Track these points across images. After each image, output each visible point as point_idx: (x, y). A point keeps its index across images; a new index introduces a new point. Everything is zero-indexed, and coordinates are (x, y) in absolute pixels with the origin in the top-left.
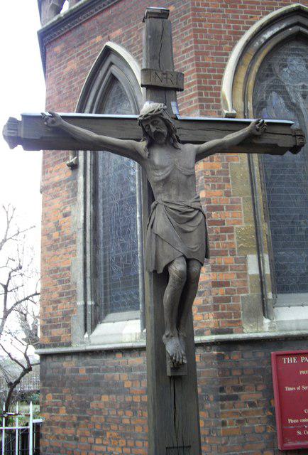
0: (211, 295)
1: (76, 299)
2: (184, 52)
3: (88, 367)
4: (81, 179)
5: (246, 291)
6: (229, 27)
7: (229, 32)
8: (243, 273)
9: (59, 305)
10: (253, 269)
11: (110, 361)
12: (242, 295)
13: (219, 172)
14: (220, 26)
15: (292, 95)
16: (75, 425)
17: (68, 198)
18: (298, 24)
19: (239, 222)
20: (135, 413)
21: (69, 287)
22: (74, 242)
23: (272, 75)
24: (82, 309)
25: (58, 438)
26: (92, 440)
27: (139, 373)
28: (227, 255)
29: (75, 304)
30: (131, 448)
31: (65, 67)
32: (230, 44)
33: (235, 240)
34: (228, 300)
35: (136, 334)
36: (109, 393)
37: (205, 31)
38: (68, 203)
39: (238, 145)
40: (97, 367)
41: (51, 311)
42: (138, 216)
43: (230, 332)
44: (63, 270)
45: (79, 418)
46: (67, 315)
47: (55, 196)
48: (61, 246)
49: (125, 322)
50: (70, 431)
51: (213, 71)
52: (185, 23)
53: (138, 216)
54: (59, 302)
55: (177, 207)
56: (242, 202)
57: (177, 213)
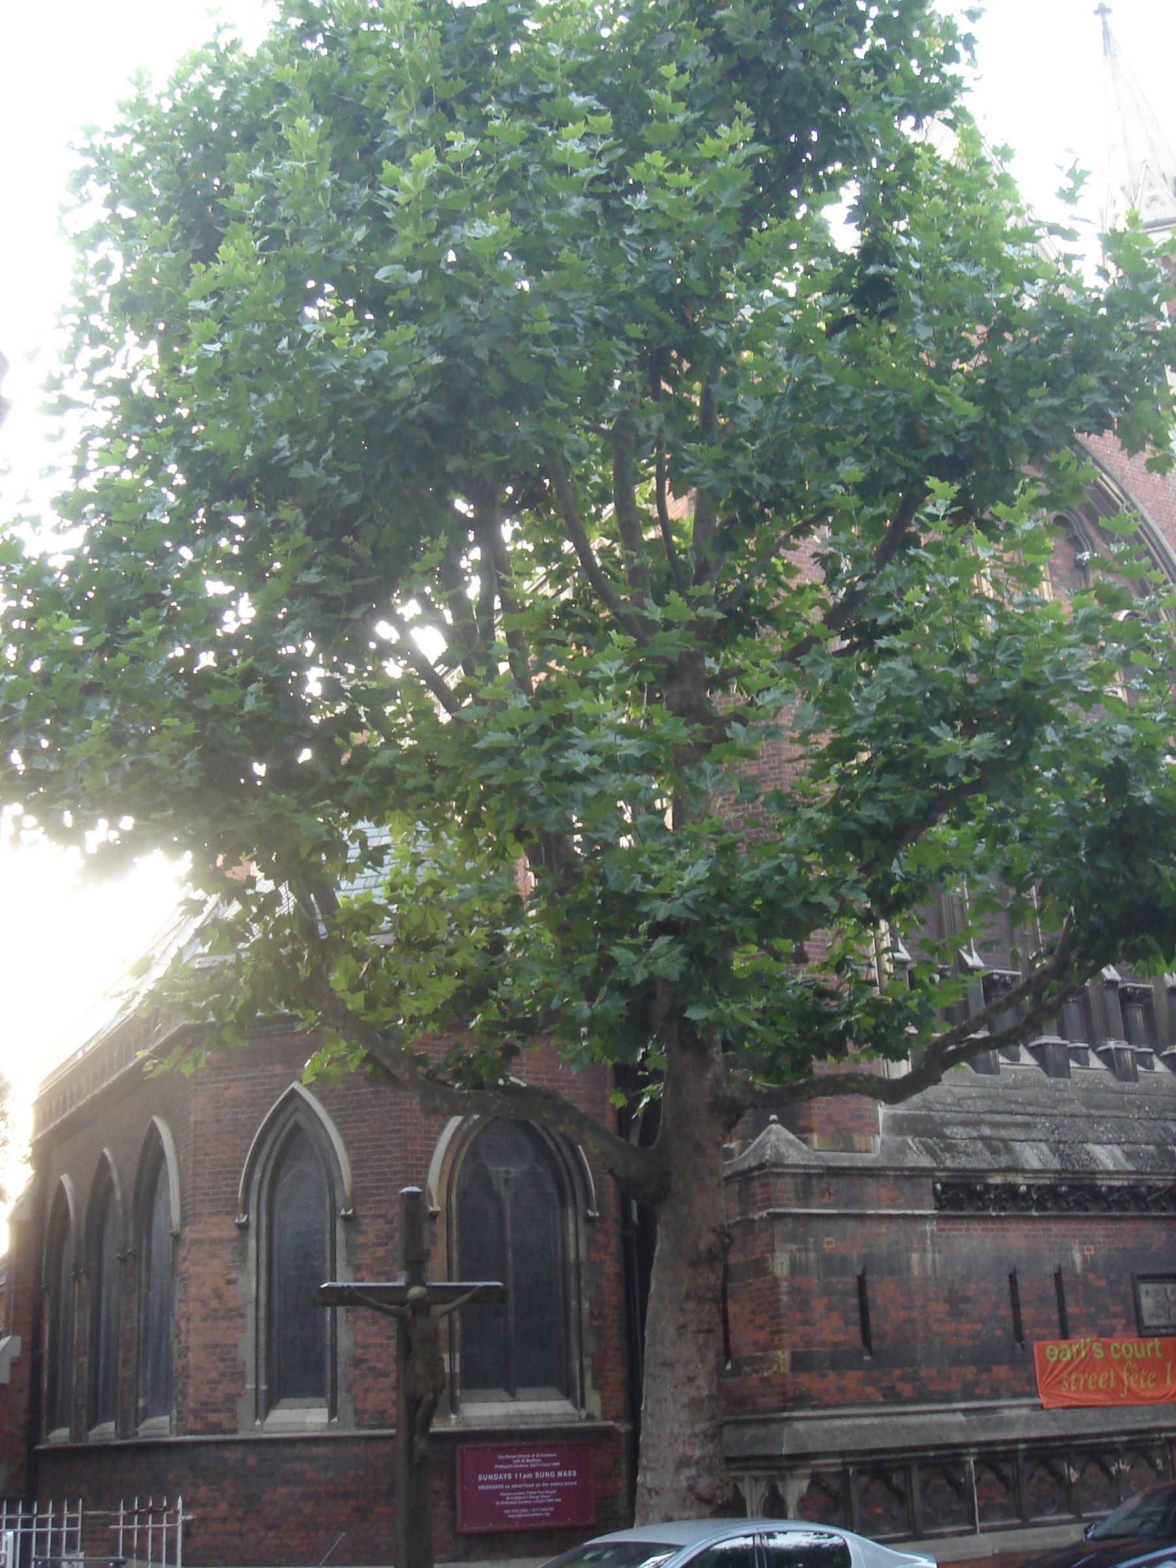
4: (252, 1243)
29: (243, 1387)
31: (227, 1088)
41: (207, 1392)
44: (226, 1346)
45: (246, 1513)
46: (231, 1399)
47: (213, 1256)
48: (223, 1318)
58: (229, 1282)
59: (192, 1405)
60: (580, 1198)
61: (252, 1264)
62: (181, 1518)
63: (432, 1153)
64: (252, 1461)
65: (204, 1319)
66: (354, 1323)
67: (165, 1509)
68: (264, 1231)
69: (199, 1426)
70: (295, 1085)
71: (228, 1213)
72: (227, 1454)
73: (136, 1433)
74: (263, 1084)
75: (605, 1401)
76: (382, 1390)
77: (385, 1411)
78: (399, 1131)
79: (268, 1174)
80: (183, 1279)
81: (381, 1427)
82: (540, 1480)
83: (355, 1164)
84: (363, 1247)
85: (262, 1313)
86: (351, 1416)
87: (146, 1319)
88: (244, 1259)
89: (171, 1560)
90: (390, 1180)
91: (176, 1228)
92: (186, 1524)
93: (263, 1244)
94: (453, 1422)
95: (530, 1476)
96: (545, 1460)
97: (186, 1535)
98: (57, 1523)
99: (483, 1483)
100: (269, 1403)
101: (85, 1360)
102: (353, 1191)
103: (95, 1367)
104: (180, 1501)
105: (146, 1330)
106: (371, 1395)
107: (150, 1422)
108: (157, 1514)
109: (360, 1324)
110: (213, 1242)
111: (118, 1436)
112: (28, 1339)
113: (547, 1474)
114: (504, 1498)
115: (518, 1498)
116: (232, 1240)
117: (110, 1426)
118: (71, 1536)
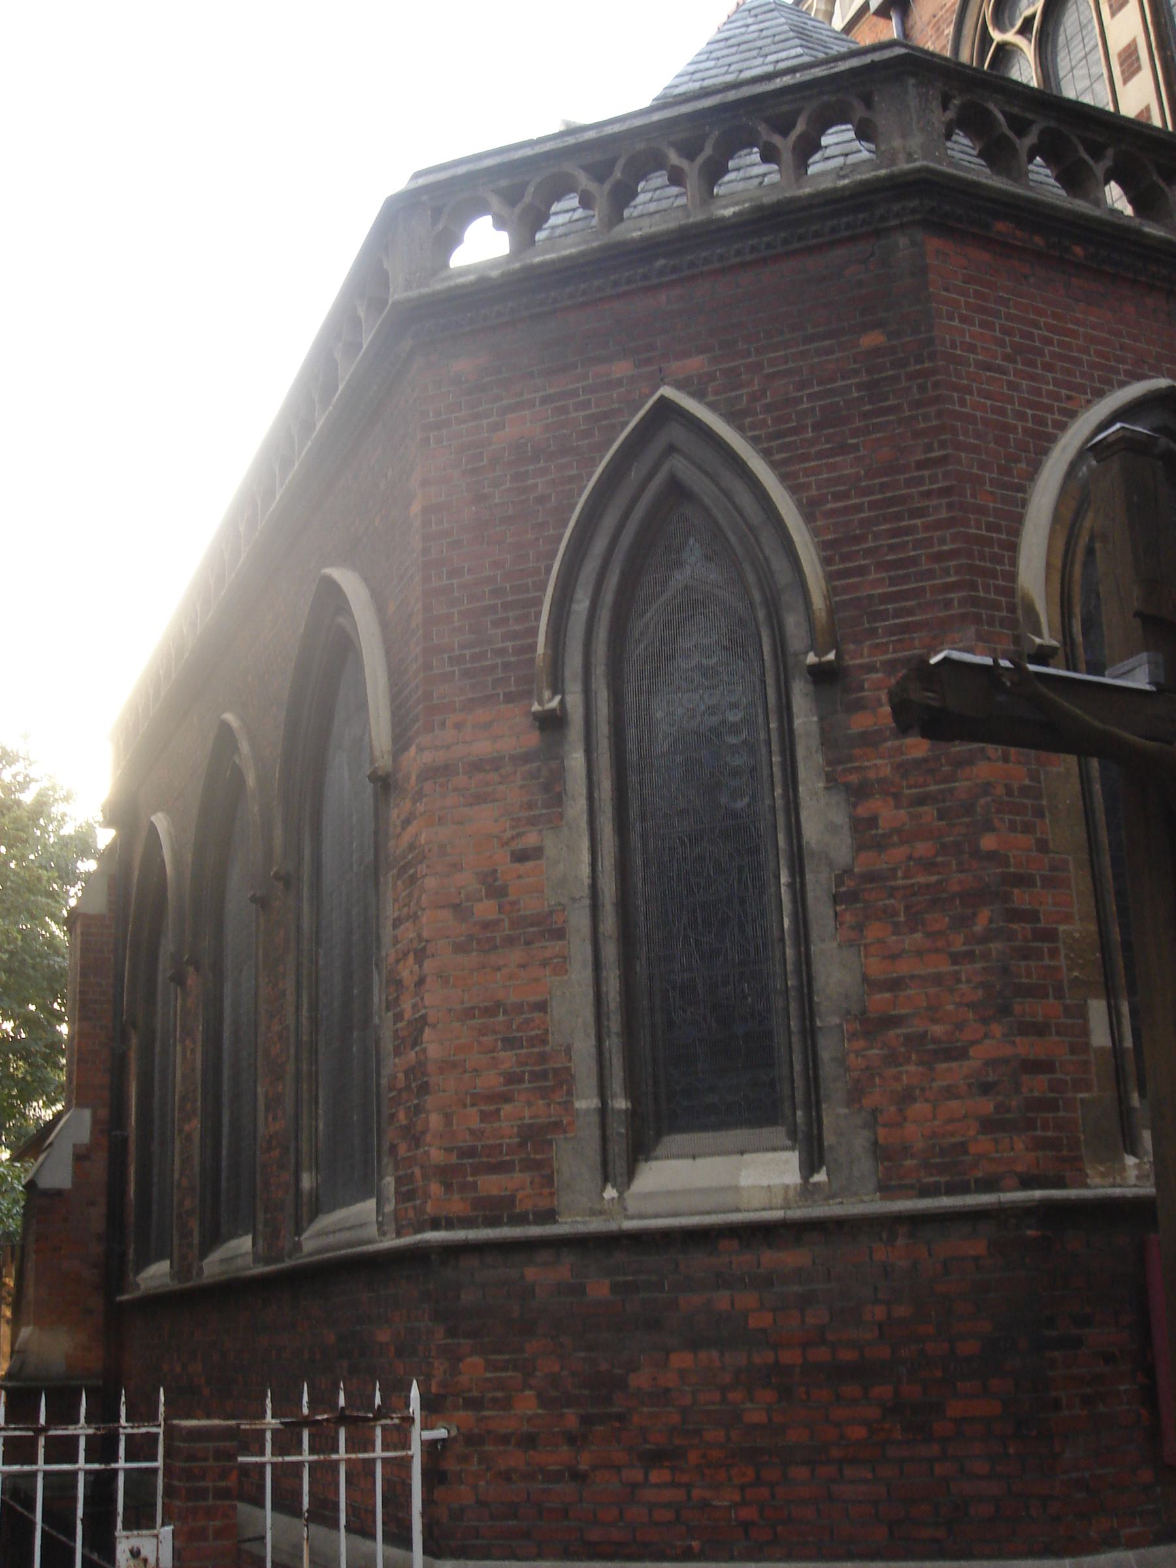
1: (570, 1093)
2: (920, 465)
3: (620, 1279)
4: (576, 759)
5: (1088, 1088)
6: (1022, 416)
7: (1025, 430)
8: (1081, 1044)
9: (507, 1109)
10: (1100, 1037)
11: (699, 1262)
12: (1081, 1095)
13: (1024, 791)
16: (571, 1439)
17: (530, 806)
19: (1067, 918)
21: (543, 1058)
22: (559, 934)
24: (595, 1119)
25: (509, 1479)
26: (636, 1475)
27: (797, 1289)
28: (1046, 996)
29: (567, 1105)
31: (497, 427)
32: (1028, 464)
33: (1062, 962)
34: (1052, 1105)
35: (787, 1187)
36: (694, 1345)
41: (475, 1123)
42: (784, 879)
43: (1061, 1184)
44: (519, 1008)
45: (587, 1420)
46: (537, 1139)
47: (481, 799)
48: (510, 941)
49: (735, 1158)
50: (558, 1457)
51: (998, 529)
52: (922, 388)
53: (784, 879)
54: (506, 1098)
56: (1071, 867)
58: (521, 856)
59: (437, 1155)
61: (577, 808)
62: (418, 1436)
63: (1019, 519)
64: (599, 1289)
66: (859, 928)
67: (380, 1414)
68: (603, 729)
69: (457, 1206)
70: (667, 391)
71: (509, 698)
72: (531, 1273)
73: (298, 1247)
74: (585, 405)
76: (950, 1093)
77: (962, 1147)
78: (943, 460)
79: (608, 598)
80: (403, 870)
81: (952, 1189)
83: (829, 550)
84: (869, 740)
85: (609, 923)
86: (865, 1165)
87: (314, 1006)
89: (399, 1536)
90: (931, 574)
91: (384, 763)
92: (430, 1447)
93: (604, 759)
94: (1132, 1174)
97: (433, 1477)
98: (103, 1448)
100: (639, 1144)
101: (195, 1125)
102: (831, 610)
103: (212, 1131)
104: (415, 1393)
105: (314, 1021)
106: (919, 1108)
107: (326, 1221)
108: (358, 1424)
109: (875, 931)
110: (477, 766)
111: (257, 1259)
112: (104, 1113)
116: (526, 758)
117: (245, 1243)
118: (140, 1483)
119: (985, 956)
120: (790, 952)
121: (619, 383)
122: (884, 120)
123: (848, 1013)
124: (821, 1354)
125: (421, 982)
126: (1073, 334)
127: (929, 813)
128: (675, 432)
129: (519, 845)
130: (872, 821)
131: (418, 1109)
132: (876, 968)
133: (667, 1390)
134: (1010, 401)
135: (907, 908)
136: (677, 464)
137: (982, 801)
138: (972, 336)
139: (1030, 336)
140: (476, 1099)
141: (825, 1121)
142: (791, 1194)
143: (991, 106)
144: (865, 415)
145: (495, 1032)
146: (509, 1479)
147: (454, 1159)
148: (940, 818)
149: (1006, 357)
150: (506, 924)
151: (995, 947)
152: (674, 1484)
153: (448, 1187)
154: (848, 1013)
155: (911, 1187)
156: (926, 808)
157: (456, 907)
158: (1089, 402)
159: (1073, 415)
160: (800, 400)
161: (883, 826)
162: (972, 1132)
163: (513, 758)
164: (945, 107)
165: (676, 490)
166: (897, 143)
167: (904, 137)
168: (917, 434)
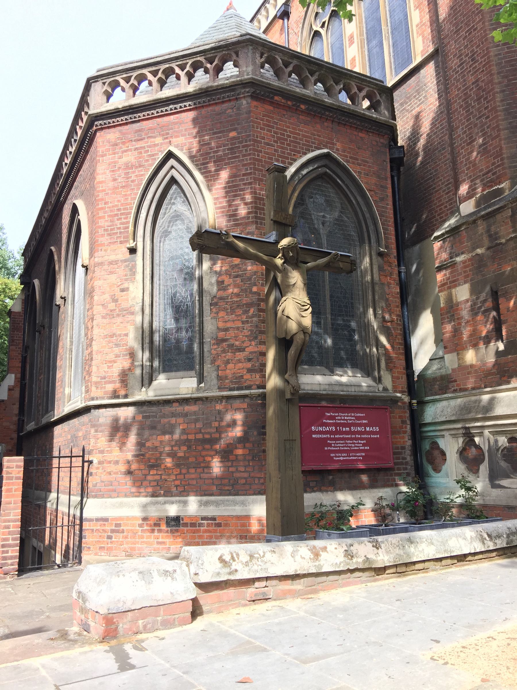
0: (258, 361)
2: (244, 175)
11: (167, 409)
14: (271, 159)
15: (316, 222)
17: (126, 275)
18: (325, 166)
20: (189, 447)
23: (303, 204)
30: (184, 474)
31: (120, 157)
37: (261, 161)
38: (126, 280)
39: (325, 266)
40: (154, 414)
41: (106, 369)
44: (120, 335)
47: (111, 273)
48: (118, 315)
52: (246, 150)
54: (115, 362)
55: (299, 302)
57: (299, 305)
58: (122, 290)
60: (373, 240)
61: (139, 277)
65: (103, 317)
66: (217, 313)
71: (121, 242)
75: (394, 379)
76: (239, 361)
81: (238, 389)
82: (355, 433)
86: (215, 382)
88: (133, 272)
95: (348, 429)
96: (358, 418)
99: (315, 433)
109: (222, 314)
110: (111, 263)
112: (19, 376)
113: (359, 429)
114: (330, 445)
115: (340, 445)
116: (125, 261)
119: (252, 322)
120: (197, 320)
121: (157, 145)
122: (241, 62)
123: (212, 338)
124: (200, 436)
125: (92, 327)
126: (299, 134)
127: (238, 280)
128: (172, 162)
129: (122, 287)
130: (223, 282)
131: (90, 366)
132: (221, 325)
133: (156, 447)
134: (274, 155)
135: (231, 308)
136: (173, 172)
137: (254, 277)
138: (264, 134)
139: (284, 135)
140: (107, 362)
141: (205, 368)
142: (194, 389)
143: (277, 57)
144: (229, 159)
145: (112, 342)
146: (110, 474)
147: (99, 380)
148: (242, 282)
149: (274, 141)
150: (117, 310)
151: (255, 319)
152: (157, 474)
153: (97, 388)
154: (212, 338)
155: (227, 388)
156: (237, 279)
157: (103, 305)
158: (301, 156)
159: (295, 160)
160: (210, 153)
161: (226, 283)
162: (245, 373)
163: (121, 261)
164: (261, 57)
165: (173, 181)
166: (244, 69)
167: (247, 67)
168: (244, 165)
